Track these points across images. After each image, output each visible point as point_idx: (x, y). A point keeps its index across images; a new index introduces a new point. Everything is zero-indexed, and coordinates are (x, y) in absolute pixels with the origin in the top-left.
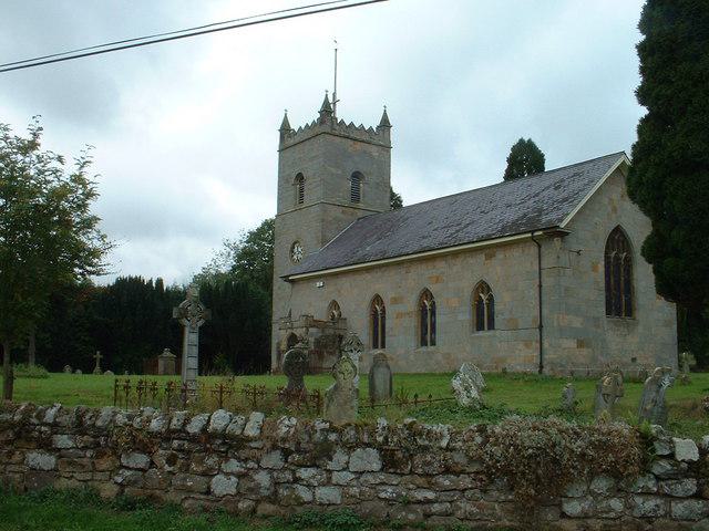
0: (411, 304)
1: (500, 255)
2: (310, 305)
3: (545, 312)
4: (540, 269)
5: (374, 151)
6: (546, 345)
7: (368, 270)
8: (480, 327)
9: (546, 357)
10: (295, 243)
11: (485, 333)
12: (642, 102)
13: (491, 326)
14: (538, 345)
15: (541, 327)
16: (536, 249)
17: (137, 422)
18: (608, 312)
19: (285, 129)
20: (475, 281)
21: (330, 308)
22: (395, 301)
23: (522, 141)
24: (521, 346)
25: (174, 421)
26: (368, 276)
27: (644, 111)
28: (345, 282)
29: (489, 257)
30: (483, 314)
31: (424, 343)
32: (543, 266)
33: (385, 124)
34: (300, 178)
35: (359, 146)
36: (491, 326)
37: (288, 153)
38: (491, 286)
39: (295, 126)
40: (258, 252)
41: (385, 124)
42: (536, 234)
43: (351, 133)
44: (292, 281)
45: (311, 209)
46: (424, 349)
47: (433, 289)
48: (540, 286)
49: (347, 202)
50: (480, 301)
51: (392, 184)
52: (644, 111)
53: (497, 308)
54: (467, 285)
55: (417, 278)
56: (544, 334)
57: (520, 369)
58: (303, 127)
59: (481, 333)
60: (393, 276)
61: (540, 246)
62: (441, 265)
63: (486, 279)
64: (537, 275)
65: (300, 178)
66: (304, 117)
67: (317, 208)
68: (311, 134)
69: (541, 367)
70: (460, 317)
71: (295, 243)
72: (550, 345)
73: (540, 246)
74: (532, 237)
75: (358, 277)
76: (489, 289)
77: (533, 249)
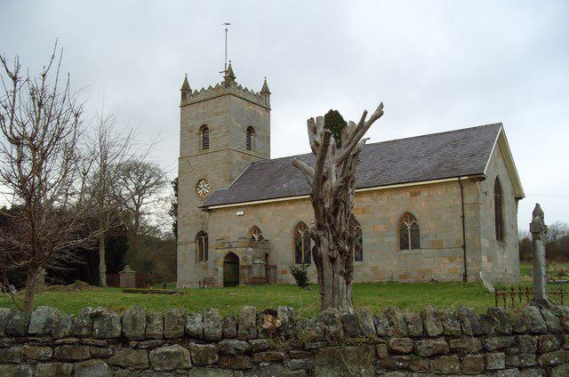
3: (467, 235)
4: (463, 205)
5: (261, 112)
6: (469, 260)
7: (291, 202)
8: (404, 246)
9: (468, 268)
10: (200, 181)
13: (416, 245)
14: (462, 260)
15: (464, 247)
16: (459, 190)
18: (497, 239)
19: (186, 89)
20: (402, 211)
25: (85, 340)
29: (414, 195)
30: (409, 237)
32: (465, 202)
33: (266, 92)
34: (204, 128)
35: (251, 107)
36: (416, 245)
39: (194, 87)
42: (462, 178)
43: (244, 95)
45: (218, 154)
48: (463, 217)
49: (244, 149)
53: (422, 233)
54: (394, 214)
57: (448, 279)
59: (405, 252)
64: (461, 209)
65: (204, 128)
66: (249, 81)
67: (224, 153)
68: (215, 94)
69: (465, 276)
70: (387, 239)
72: (473, 260)
73: (462, 188)
74: (459, 181)
76: (259, 231)
77: (457, 190)
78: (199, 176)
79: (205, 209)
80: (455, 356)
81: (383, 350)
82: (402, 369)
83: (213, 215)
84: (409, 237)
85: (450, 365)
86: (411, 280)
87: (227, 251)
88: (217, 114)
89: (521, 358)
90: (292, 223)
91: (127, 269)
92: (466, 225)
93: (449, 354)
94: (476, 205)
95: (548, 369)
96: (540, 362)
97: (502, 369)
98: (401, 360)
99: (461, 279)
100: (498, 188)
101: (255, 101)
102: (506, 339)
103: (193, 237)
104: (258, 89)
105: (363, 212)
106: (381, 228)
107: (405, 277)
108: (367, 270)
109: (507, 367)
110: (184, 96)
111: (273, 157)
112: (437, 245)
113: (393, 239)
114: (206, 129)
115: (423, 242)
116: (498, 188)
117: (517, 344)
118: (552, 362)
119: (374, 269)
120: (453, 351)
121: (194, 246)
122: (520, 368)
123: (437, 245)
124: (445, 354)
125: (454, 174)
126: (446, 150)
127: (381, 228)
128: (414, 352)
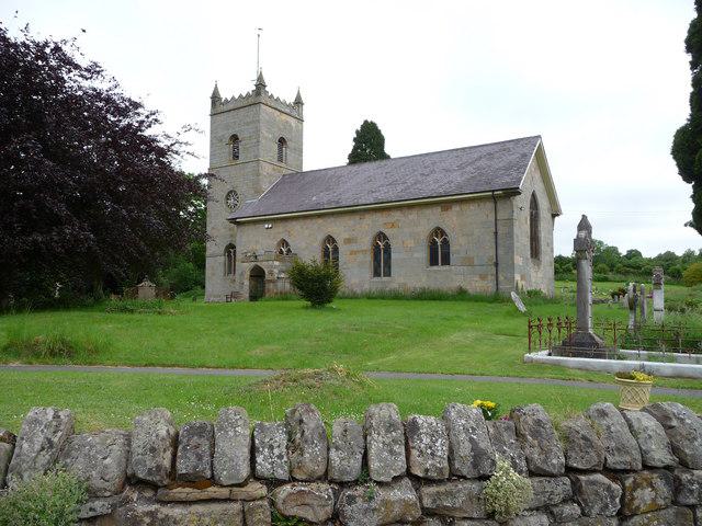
0: (366, 243)
1: (456, 208)
2: (257, 242)
3: (500, 252)
5: (293, 122)
6: (501, 278)
12: (630, 252)
13: (446, 261)
15: (496, 265)
18: (532, 257)
19: (215, 98)
20: (432, 226)
21: (278, 244)
22: (348, 241)
23: (366, 122)
26: (320, 221)
27: (623, 252)
28: (296, 227)
30: (439, 252)
33: (298, 102)
34: (235, 138)
35: (284, 117)
36: (446, 261)
37: (218, 117)
38: (447, 231)
39: (225, 95)
40: (388, 157)
41: (298, 102)
44: (239, 224)
46: (376, 279)
47: (387, 232)
49: (275, 161)
52: (623, 252)
55: (376, 223)
56: (500, 268)
58: (237, 97)
59: (435, 268)
60: (349, 221)
61: (496, 203)
62: (396, 215)
63: (443, 227)
65: (235, 138)
68: (245, 103)
70: (416, 255)
71: (231, 192)
73: (496, 203)
75: (308, 221)
83: (242, 228)
88: (248, 124)
90: (321, 237)
92: (499, 242)
94: (510, 221)
101: (287, 111)
104: (291, 99)
110: (214, 103)
111: (306, 168)
115: (453, 258)
123: (468, 262)
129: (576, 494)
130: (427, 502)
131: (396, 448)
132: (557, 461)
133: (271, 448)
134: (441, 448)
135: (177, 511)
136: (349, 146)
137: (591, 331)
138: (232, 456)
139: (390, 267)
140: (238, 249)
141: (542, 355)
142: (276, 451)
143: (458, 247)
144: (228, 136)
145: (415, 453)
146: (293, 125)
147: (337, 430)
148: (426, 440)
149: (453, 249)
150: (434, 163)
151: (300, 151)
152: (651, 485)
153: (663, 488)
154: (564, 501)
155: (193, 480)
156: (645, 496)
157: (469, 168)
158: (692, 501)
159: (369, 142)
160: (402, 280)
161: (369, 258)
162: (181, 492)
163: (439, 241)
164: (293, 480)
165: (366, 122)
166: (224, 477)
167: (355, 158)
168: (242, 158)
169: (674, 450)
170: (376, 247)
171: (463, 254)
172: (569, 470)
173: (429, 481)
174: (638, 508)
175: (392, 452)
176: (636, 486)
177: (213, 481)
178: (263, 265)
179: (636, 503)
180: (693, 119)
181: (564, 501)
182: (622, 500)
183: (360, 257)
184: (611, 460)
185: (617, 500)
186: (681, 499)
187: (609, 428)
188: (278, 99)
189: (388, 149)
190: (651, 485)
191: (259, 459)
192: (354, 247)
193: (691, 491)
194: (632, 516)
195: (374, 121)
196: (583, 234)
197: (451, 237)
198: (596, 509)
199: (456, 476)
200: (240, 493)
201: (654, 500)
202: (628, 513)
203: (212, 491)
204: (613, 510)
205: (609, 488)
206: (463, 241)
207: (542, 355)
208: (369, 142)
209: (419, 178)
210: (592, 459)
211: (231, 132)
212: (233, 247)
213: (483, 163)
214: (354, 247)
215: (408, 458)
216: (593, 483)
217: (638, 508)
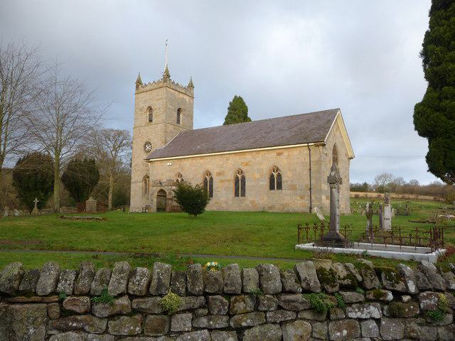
0: (230, 176)
3: (313, 182)
5: (187, 98)
6: (313, 198)
11: (276, 191)
14: (309, 198)
15: (310, 189)
17: (198, 283)
19: (139, 82)
22: (219, 174)
23: (236, 97)
24: (298, 198)
29: (279, 154)
31: (237, 194)
33: (191, 86)
35: (181, 95)
36: (280, 187)
37: (140, 96)
39: (144, 81)
41: (191, 86)
43: (176, 87)
47: (244, 168)
49: (175, 123)
50: (272, 176)
51: (428, 150)
59: (272, 191)
61: (283, 287)
65: (150, 109)
66: (181, 79)
68: (156, 86)
69: (311, 208)
70: (261, 183)
71: (147, 143)
72: (316, 198)
74: (308, 146)
78: (146, 140)
79: (148, 160)
80: (138, 317)
81: (55, 310)
82: (75, 329)
84: (275, 182)
85: (128, 326)
86: (276, 211)
87: (159, 188)
88: (159, 99)
89: (209, 320)
90: (202, 171)
91: (91, 199)
93: (129, 315)
94: (319, 162)
95: (240, 331)
96: (232, 324)
97: (188, 331)
98: (76, 321)
99: (308, 211)
100: (335, 151)
101: (183, 91)
102: (193, 300)
103: (141, 178)
104: (186, 84)
105: (246, 165)
106: (258, 176)
107: (270, 208)
108: (248, 202)
109: (195, 329)
110: (137, 87)
111: (195, 127)
112: (293, 188)
113: (266, 183)
114: (151, 109)
116: (335, 151)
117: (206, 305)
118: (244, 324)
119: (253, 202)
120: (134, 312)
121: (141, 184)
122: (210, 330)
123: (293, 188)
124: (123, 315)
125: (305, 141)
126: (301, 126)
127: (258, 176)
128: (90, 312)
129: (206, 305)
130: (134, 306)
131: (122, 281)
132: (199, 288)
133: (66, 280)
134: (144, 281)
135: (17, 306)
136: (226, 113)
137: (338, 232)
138: (46, 283)
139: (245, 191)
140: (150, 178)
141: (308, 246)
142: (68, 282)
143: (287, 179)
144: (146, 108)
145: (131, 283)
146: (187, 100)
147: (98, 273)
148: (138, 278)
149: (284, 179)
150: (274, 125)
151: (191, 117)
152: (244, 301)
153: (250, 303)
154: (200, 307)
155: (26, 293)
156: (240, 306)
157: (295, 129)
158: (264, 309)
159: (238, 111)
160: (252, 199)
161: (232, 185)
162: (20, 298)
163: (275, 174)
164: (73, 294)
165: (236, 97)
166: (39, 292)
167: (230, 120)
168: (154, 120)
169: (260, 285)
170: (237, 179)
171: (289, 183)
172: (206, 294)
173: (137, 297)
174: (236, 311)
175: (119, 283)
176: (236, 301)
177: (35, 294)
178: (165, 189)
179: (235, 309)
180: (423, 101)
181: (200, 307)
182: (229, 308)
183: (226, 184)
184: (225, 289)
185: (226, 307)
186: (260, 308)
187: (229, 274)
188: (177, 85)
189: (249, 115)
190: (244, 301)
191: (59, 286)
192: (223, 178)
193: (264, 304)
194: (235, 315)
195: (428, 13)
196: (333, 174)
197: (247, 176)
198: (216, 312)
199: (148, 295)
200: (47, 299)
201: (245, 308)
202: (231, 313)
203: (33, 298)
204: (223, 312)
205: (222, 302)
206: (289, 174)
207: (308, 246)
208: (238, 111)
209: (264, 135)
210: (216, 288)
211: (148, 105)
212: (148, 177)
213: (301, 126)
214: (223, 178)
215: (128, 284)
216: (214, 299)
217: (236, 311)
